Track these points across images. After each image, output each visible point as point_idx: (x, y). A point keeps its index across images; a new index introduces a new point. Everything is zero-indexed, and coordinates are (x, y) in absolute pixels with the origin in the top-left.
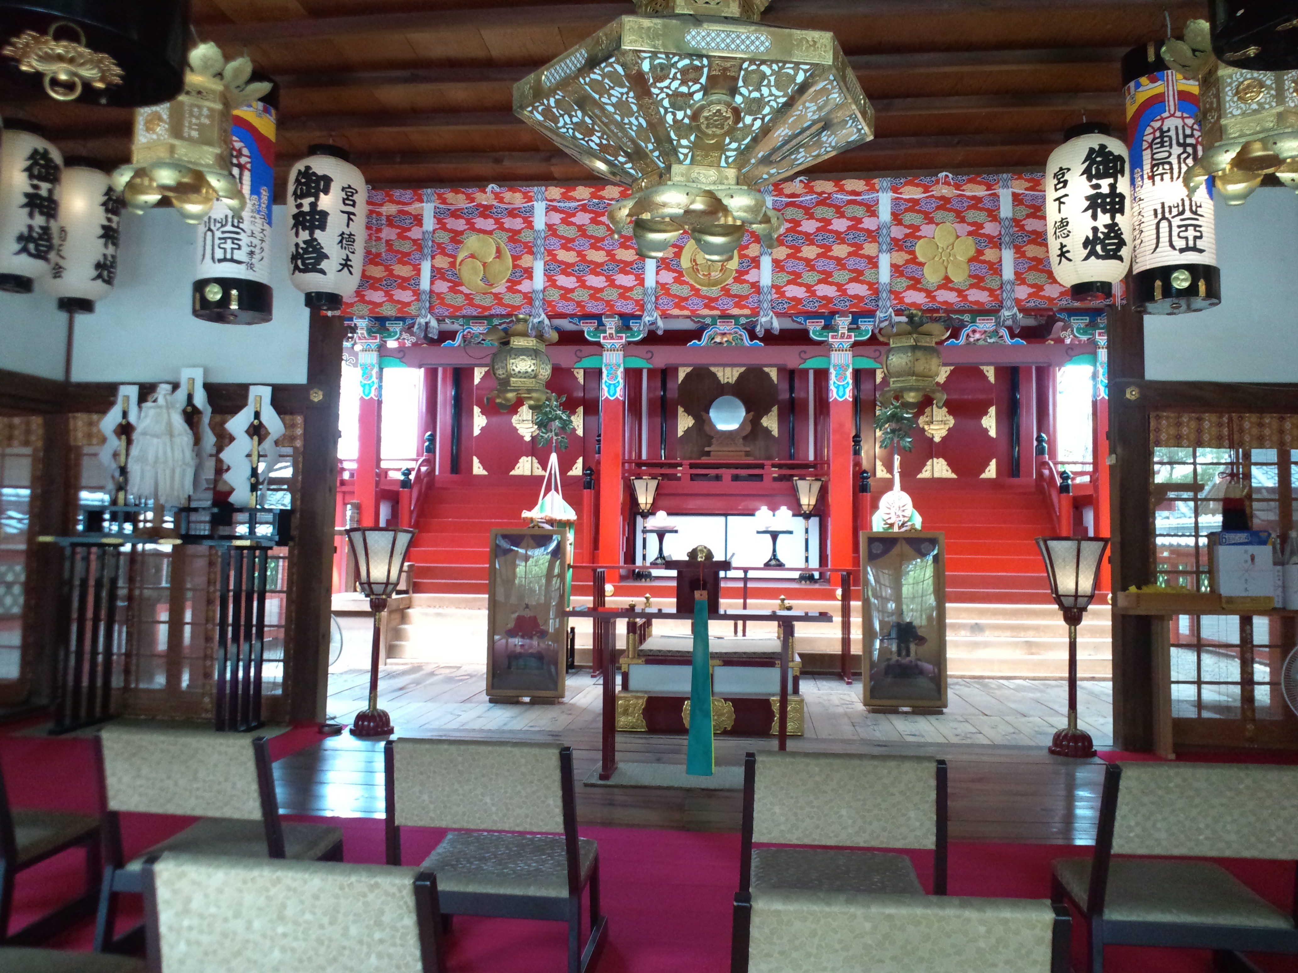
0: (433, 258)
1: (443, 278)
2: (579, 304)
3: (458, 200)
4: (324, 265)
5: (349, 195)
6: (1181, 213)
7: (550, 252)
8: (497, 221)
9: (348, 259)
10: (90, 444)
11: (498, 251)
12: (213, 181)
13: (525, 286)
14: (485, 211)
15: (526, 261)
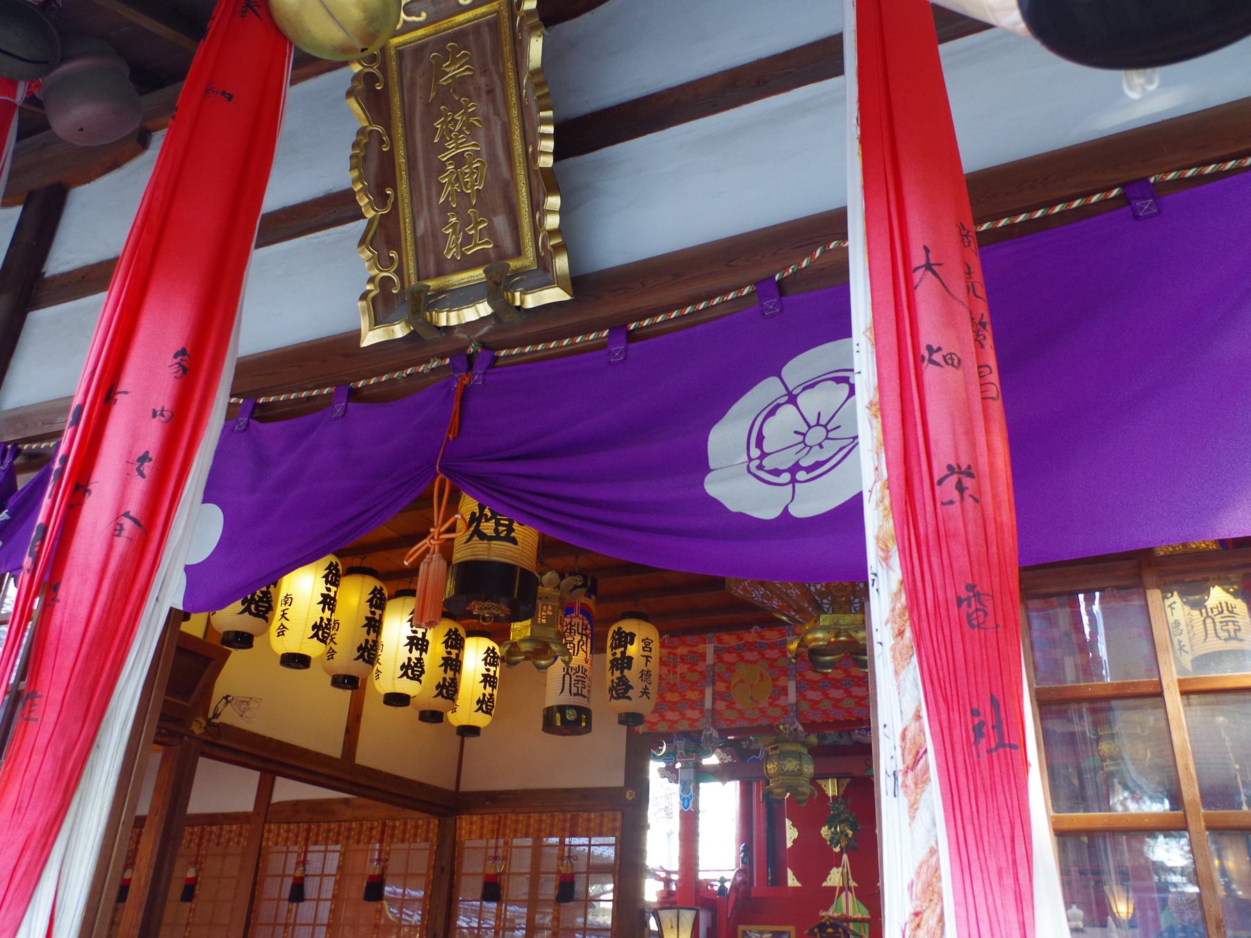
0: (714, 684)
1: (722, 699)
2: (825, 712)
3: (730, 640)
4: (630, 693)
5: (647, 644)
6: (1222, 612)
7: (800, 674)
8: (760, 653)
9: (646, 688)
10: (470, 839)
11: (762, 675)
12: (554, 647)
13: (782, 702)
14: (751, 646)
15: (782, 681)
